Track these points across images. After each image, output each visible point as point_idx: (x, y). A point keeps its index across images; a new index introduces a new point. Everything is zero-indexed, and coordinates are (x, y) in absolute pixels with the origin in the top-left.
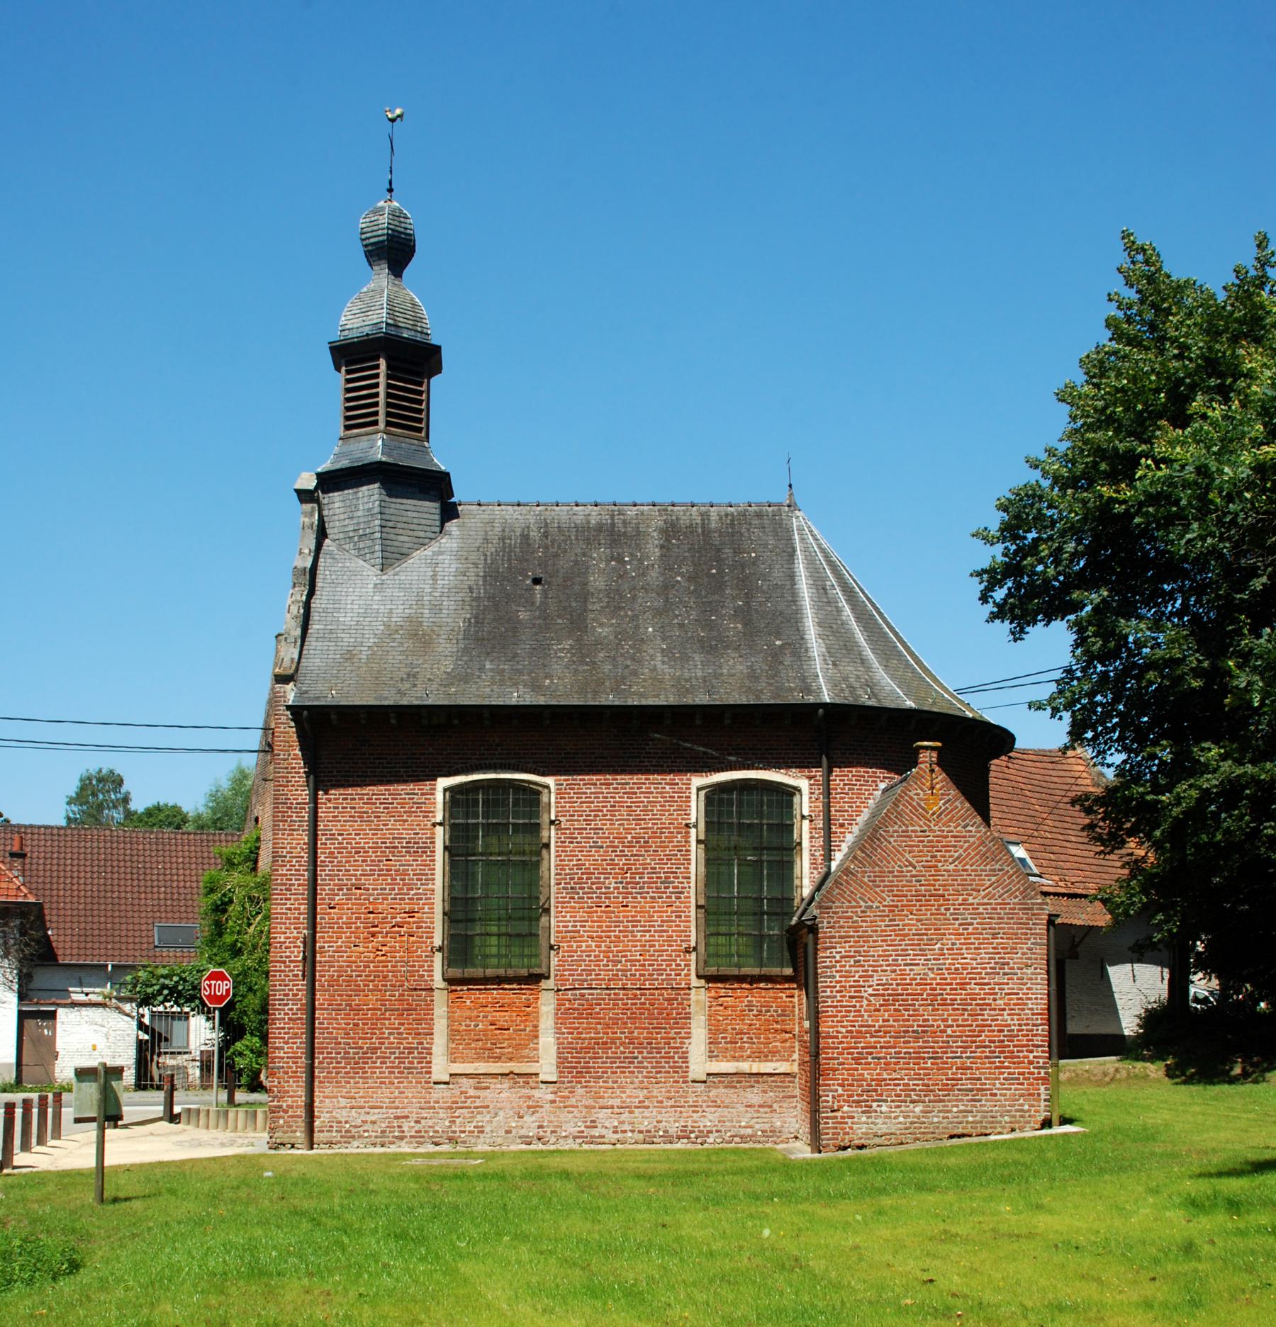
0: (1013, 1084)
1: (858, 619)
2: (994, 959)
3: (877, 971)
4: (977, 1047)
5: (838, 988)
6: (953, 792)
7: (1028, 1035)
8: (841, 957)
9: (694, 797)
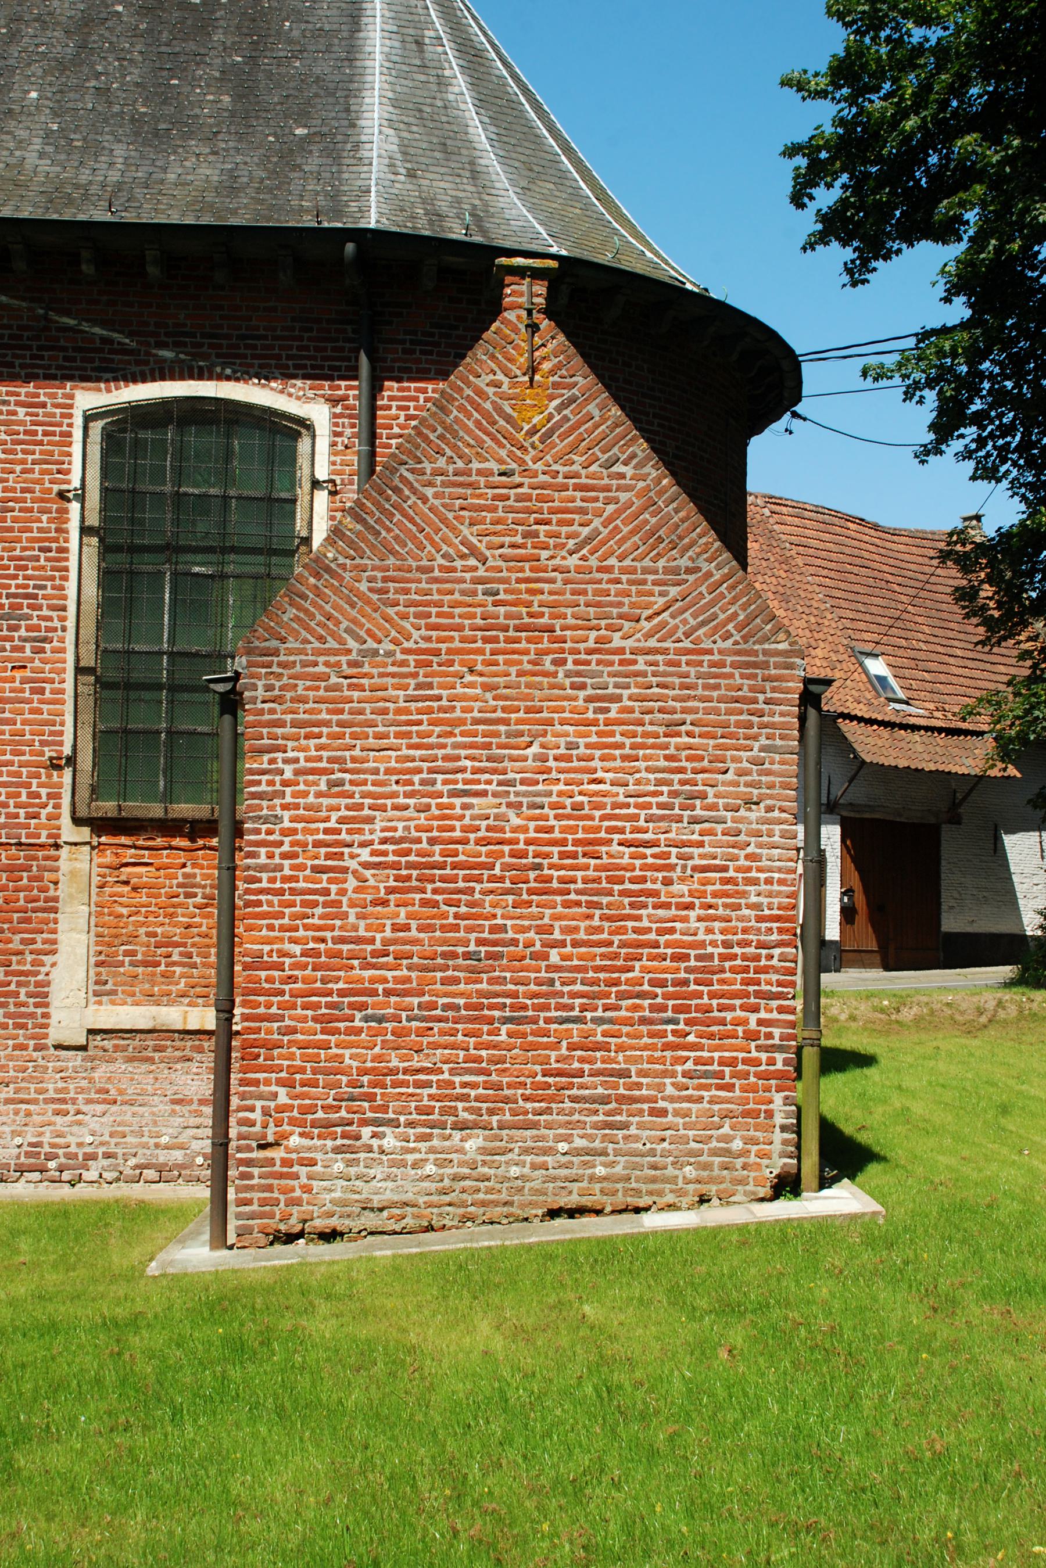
0: (707, 1087)
1: (482, 103)
2: (669, 783)
3: (383, 809)
4: (620, 996)
5: (286, 848)
6: (583, 380)
7: (746, 970)
8: (297, 772)
9: (78, 434)
